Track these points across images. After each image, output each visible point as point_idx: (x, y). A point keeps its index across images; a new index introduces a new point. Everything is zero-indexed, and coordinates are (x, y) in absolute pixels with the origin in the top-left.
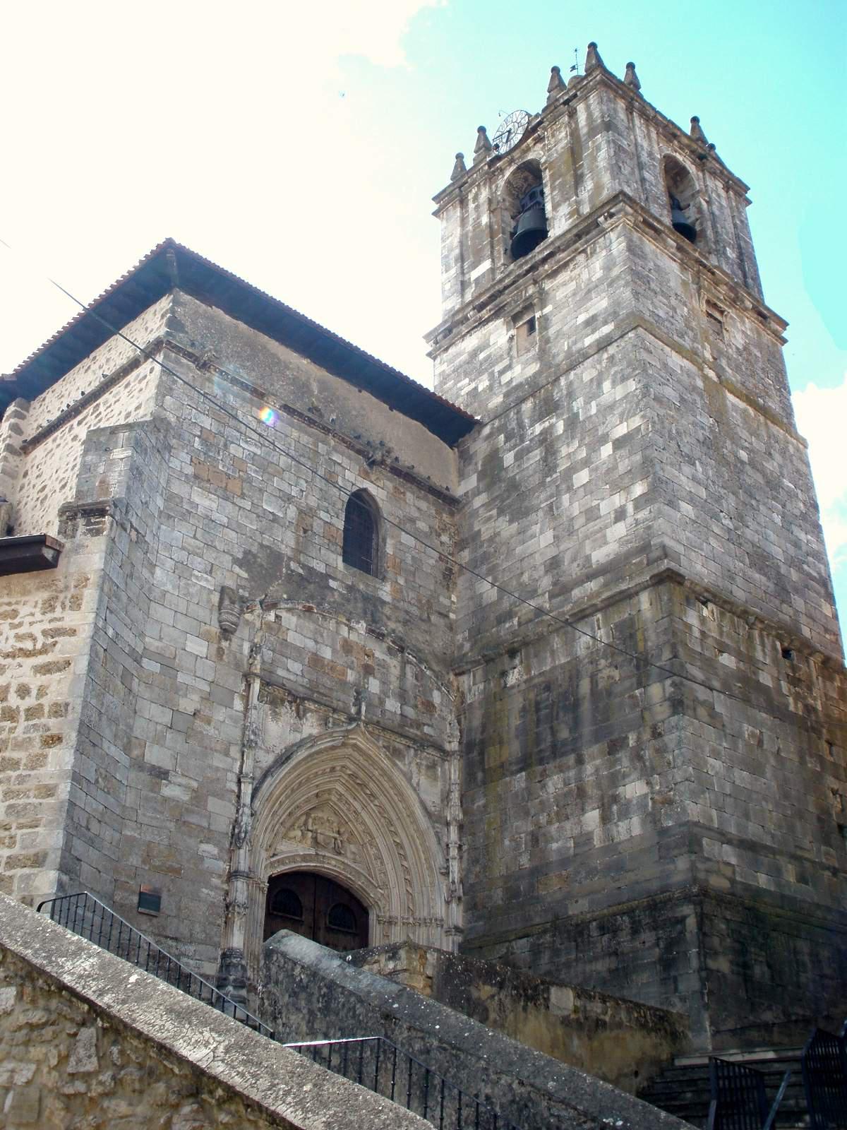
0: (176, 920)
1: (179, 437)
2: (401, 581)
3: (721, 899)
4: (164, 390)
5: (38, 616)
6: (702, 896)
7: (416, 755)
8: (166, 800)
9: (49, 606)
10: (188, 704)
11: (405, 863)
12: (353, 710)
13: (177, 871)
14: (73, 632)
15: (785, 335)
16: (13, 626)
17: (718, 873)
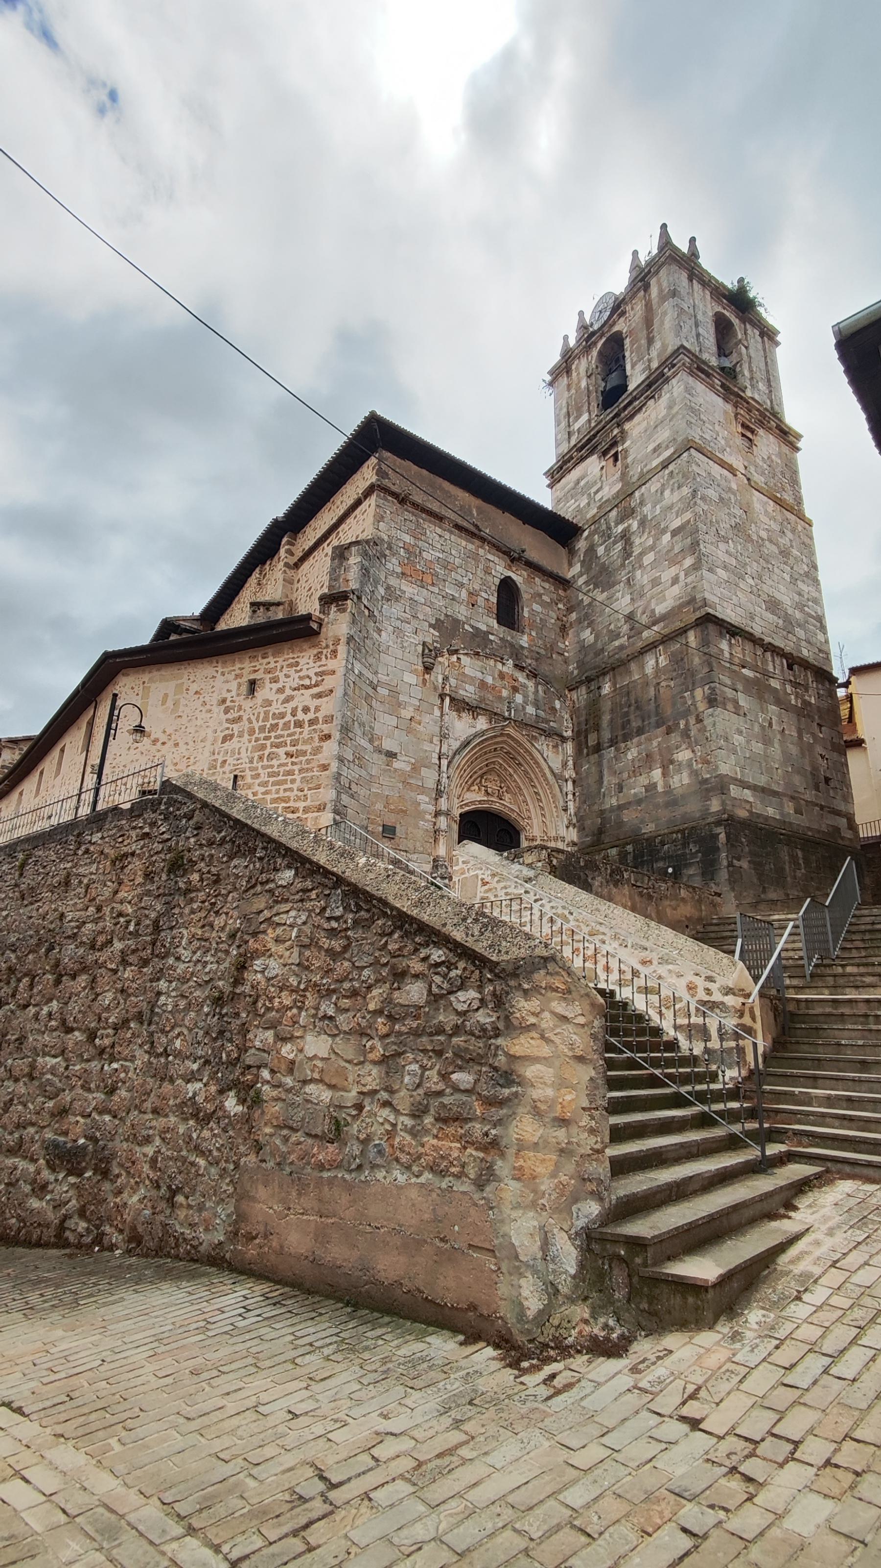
1: (390, 548)
2: (534, 634)
3: (745, 824)
4: (379, 518)
5: (312, 664)
6: (730, 822)
8: (396, 770)
9: (318, 657)
10: (407, 713)
12: (507, 714)
13: (405, 812)
14: (333, 672)
15: (799, 445)
16: (297, 671)
17: (740, 806)
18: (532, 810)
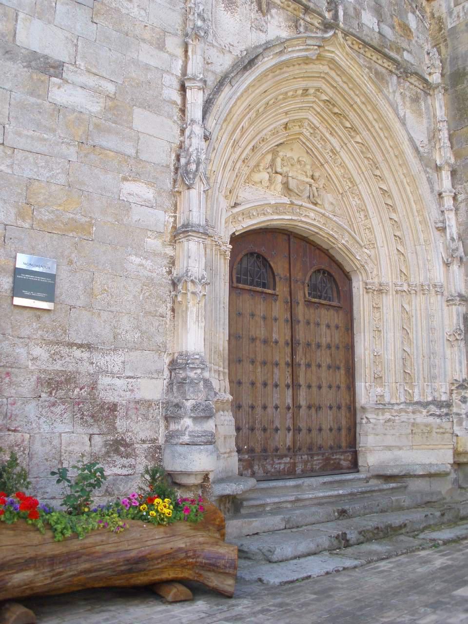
0: (86, 315)
7: (399, 83)
8: (58, 109)
11: (394, 216)
12: (328, 15)
18: (378, 229)
